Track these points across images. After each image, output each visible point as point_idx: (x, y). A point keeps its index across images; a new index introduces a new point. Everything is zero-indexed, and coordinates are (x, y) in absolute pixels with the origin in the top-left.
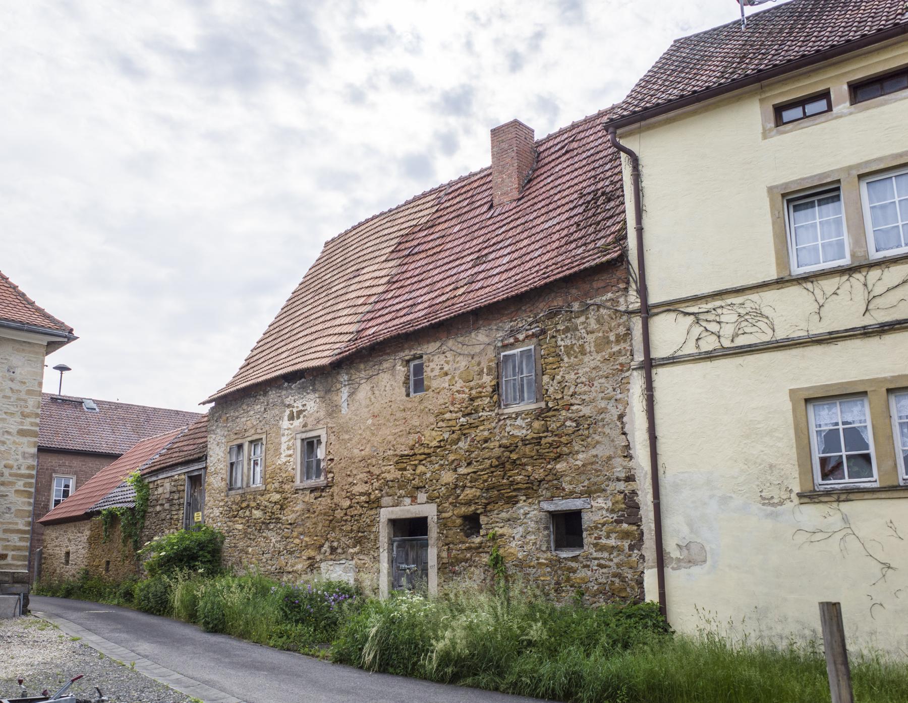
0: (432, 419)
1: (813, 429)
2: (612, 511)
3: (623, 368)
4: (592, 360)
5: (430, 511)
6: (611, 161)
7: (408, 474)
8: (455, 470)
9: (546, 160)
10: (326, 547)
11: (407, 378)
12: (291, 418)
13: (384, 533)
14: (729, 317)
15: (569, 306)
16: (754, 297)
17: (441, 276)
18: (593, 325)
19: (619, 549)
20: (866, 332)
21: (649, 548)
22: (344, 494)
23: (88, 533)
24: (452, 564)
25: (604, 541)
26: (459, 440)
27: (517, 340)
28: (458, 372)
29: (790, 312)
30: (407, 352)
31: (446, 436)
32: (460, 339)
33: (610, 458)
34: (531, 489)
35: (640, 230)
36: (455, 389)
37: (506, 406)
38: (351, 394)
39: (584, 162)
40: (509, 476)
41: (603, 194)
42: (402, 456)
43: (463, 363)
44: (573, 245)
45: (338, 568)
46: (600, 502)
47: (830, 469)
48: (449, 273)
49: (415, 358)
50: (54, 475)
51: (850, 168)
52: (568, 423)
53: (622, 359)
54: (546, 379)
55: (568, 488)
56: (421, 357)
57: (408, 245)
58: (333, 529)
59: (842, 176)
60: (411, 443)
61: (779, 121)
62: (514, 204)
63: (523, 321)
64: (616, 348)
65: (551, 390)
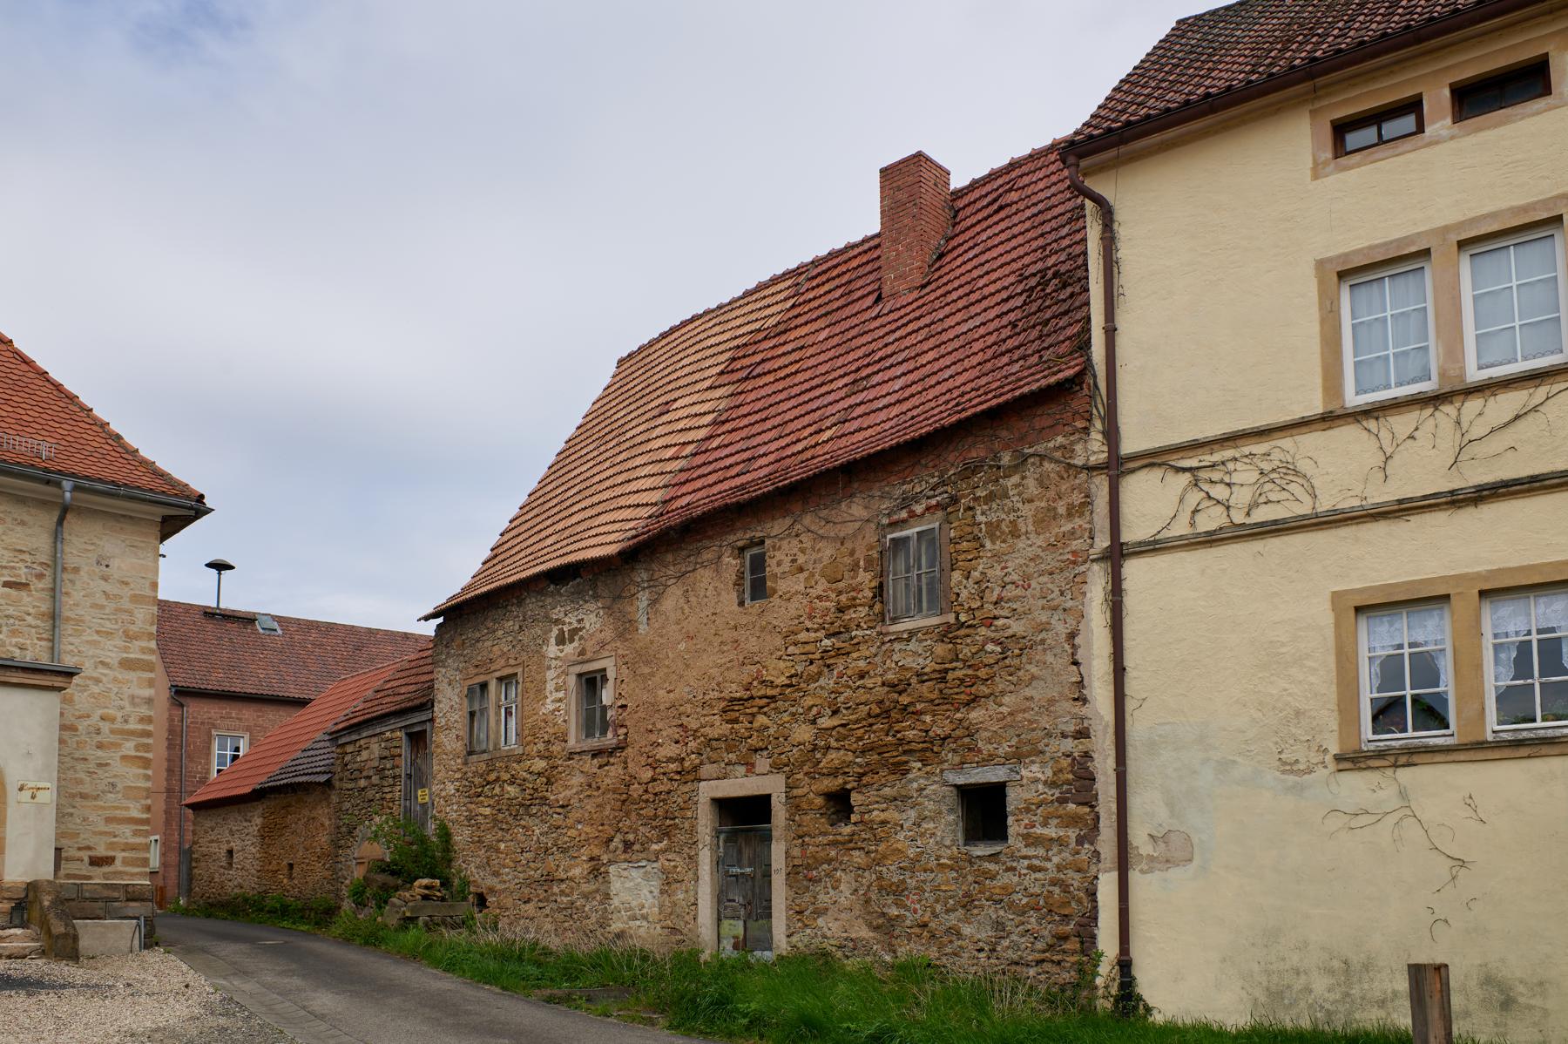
23: (258, 821)
50: (214, 732)
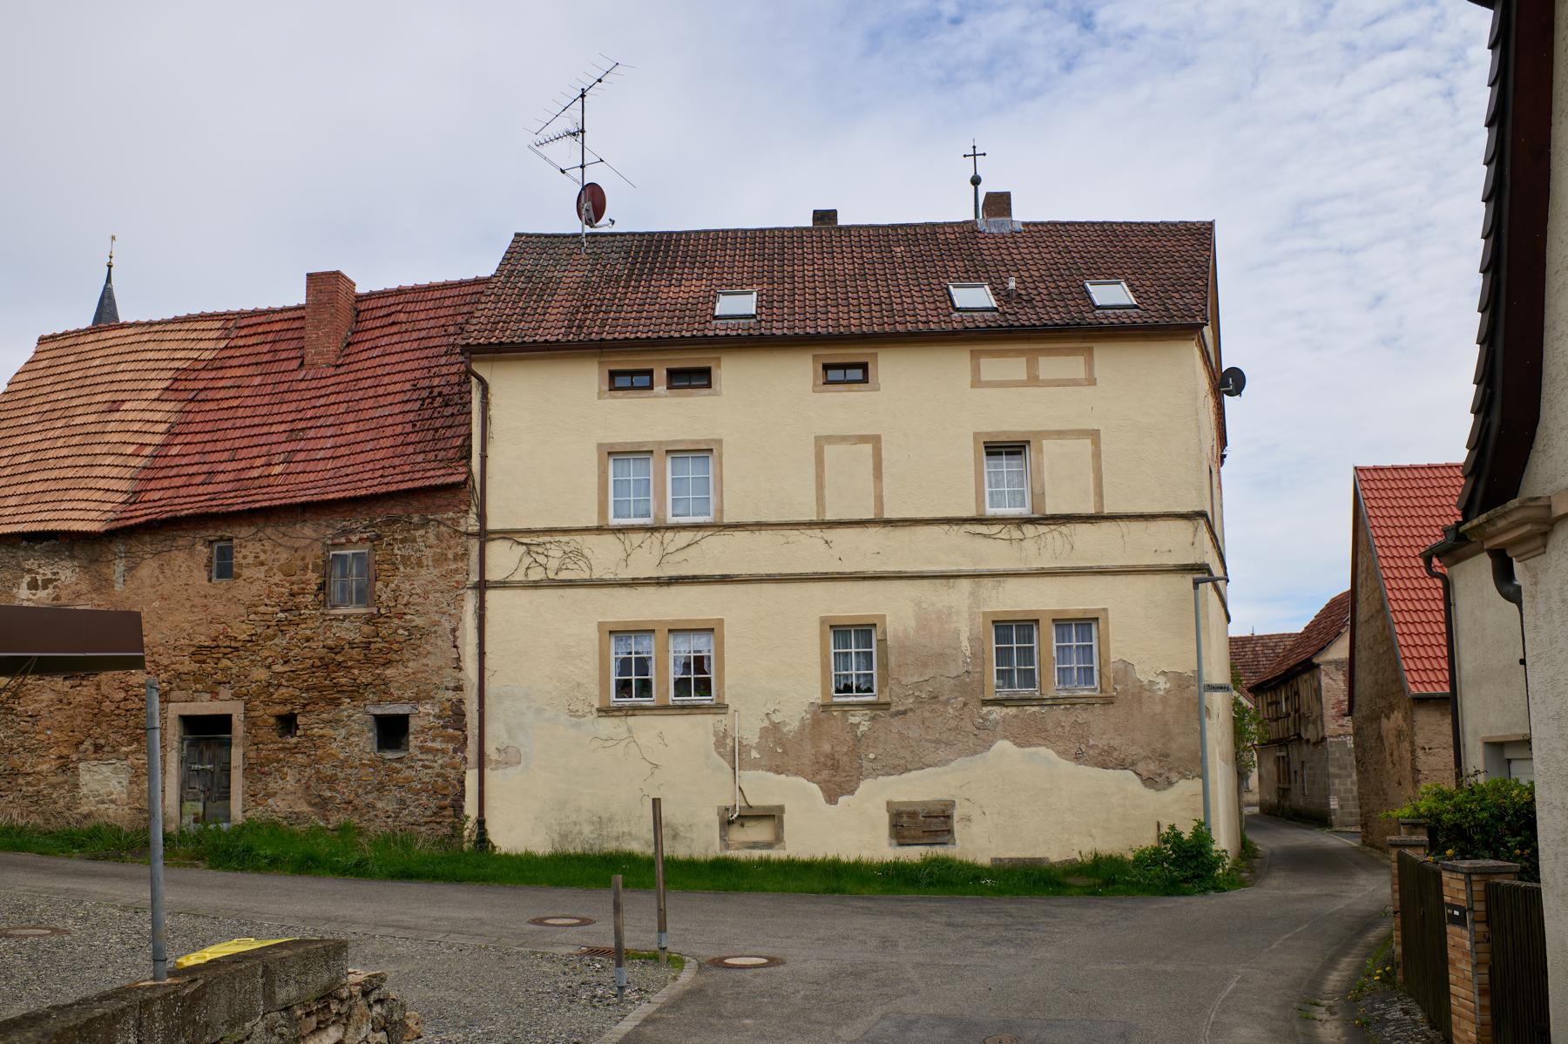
0: (242, 610)
1: (613, 656)
2: (439, 717)
3: (459, 586)
4: (428, 574)
5: (235, 709)
6: (446, 354)
7: (209, 667)
8: (269, 667)
9: (369, 324)
10: (87, 744)
11: (210, 560)
12: (33, 585)
13: (174, 732)
14: (555, 552)
15: (409, 516)
16: (578, 538)
17: (245, 442)
18: (432, 540)
19: (443, 751)
20: (660, 582)
21: (471, 751)
22: (116, 684)
24: (262, 765)
25: (429, 744)
26: (275, 636)
27: (349, 541)
28: (277, 564)
29: (604, 556)
30: (211, 532)
31: (259, 631)
32: (282, 529)
33: (440, 668)
34: (356, 691)
35: (484, 458)
36: (272, 581)
37: (334, 607)
38: (129, 569)
39: (415, 345)
40: (330, 680)
41: (440, 394)
42: (201, 647)
43: (284, 555)
44: (410, 449)
45: (104, 769)
46: (426, 708)
47: (623, 688)
48: (256, 441)
49: (221, 539)
51: (660, 443)
52: (401, 631)
53: (458, 577)
54: (379, 585)
55: (396, 693)
56: (231, 539)
57: (190, 385)
58: (99, 724)
59: (655, 449)
60: (213, 634)
61: (613, 388)
62: (331, 371)
63: (358, 523)
64: (454, 566)
65: (384, 597)
